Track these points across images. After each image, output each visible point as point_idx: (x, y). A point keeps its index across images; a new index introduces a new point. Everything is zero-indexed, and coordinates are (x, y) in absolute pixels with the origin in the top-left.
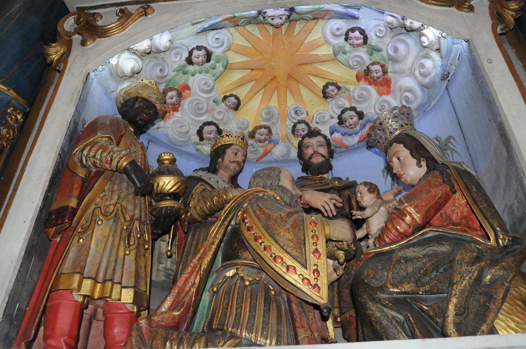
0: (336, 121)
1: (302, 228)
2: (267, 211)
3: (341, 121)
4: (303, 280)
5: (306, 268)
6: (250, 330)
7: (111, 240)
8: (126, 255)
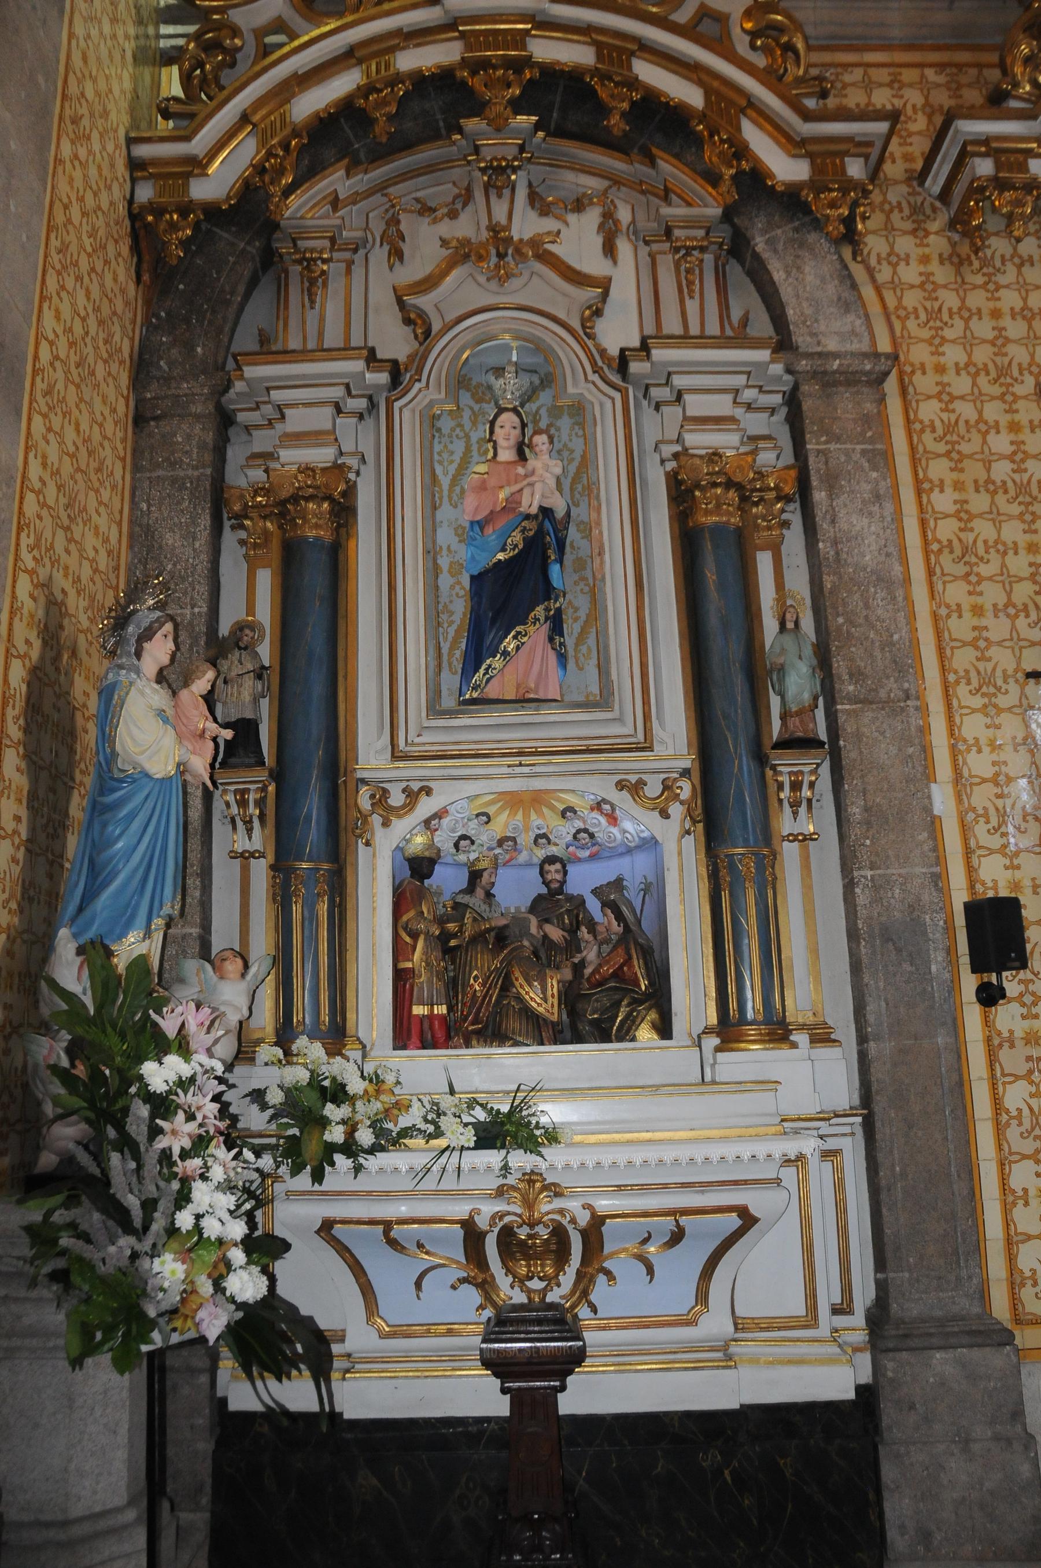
0: (570, 838)
3: (575, 837)
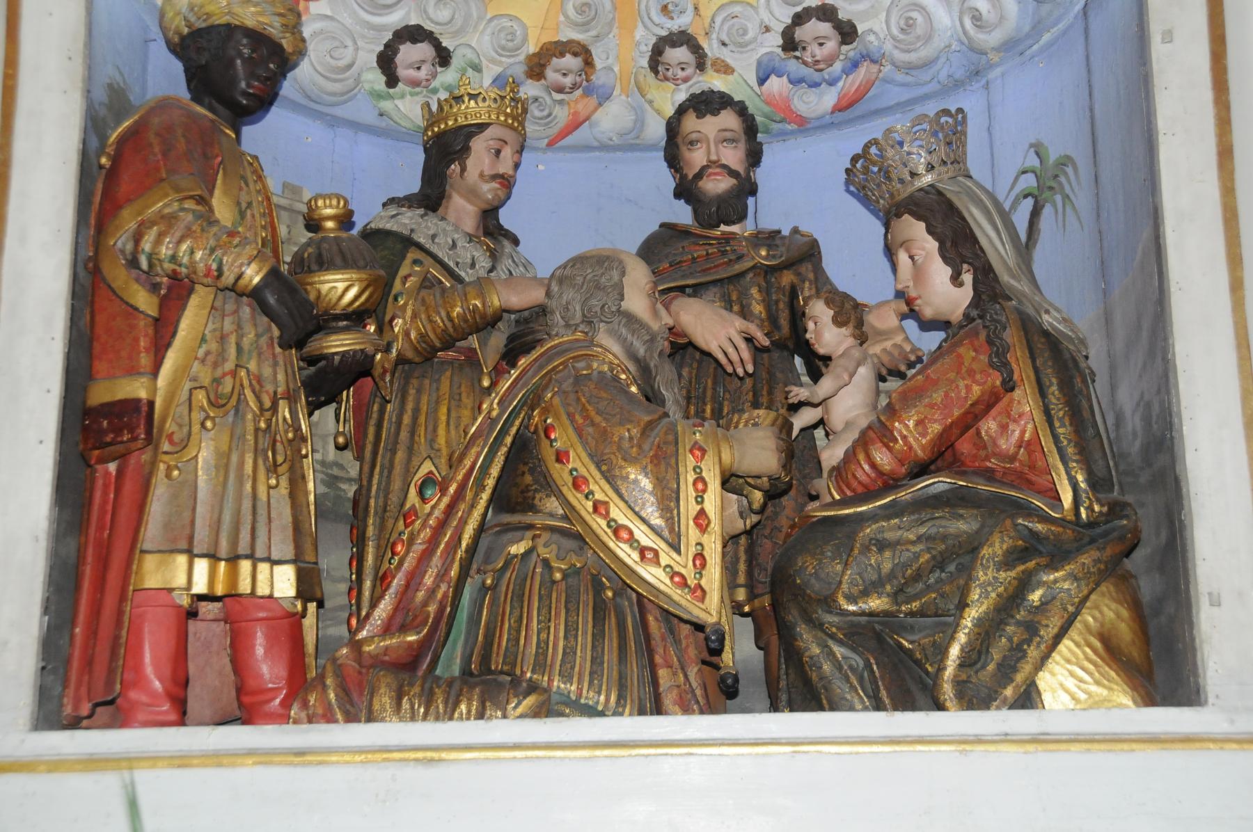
0: (774, 41)
1: (673, 461)
2: (598, 419)
3: (790, 44)
4: (672, 578)
5: (679, 552)
6: (567, 677)
7: (234, 458)
8: (270, 487)
